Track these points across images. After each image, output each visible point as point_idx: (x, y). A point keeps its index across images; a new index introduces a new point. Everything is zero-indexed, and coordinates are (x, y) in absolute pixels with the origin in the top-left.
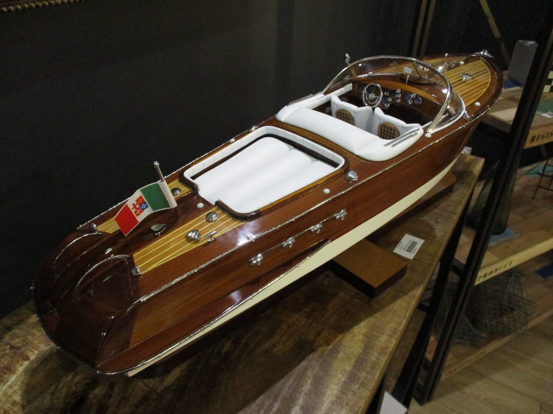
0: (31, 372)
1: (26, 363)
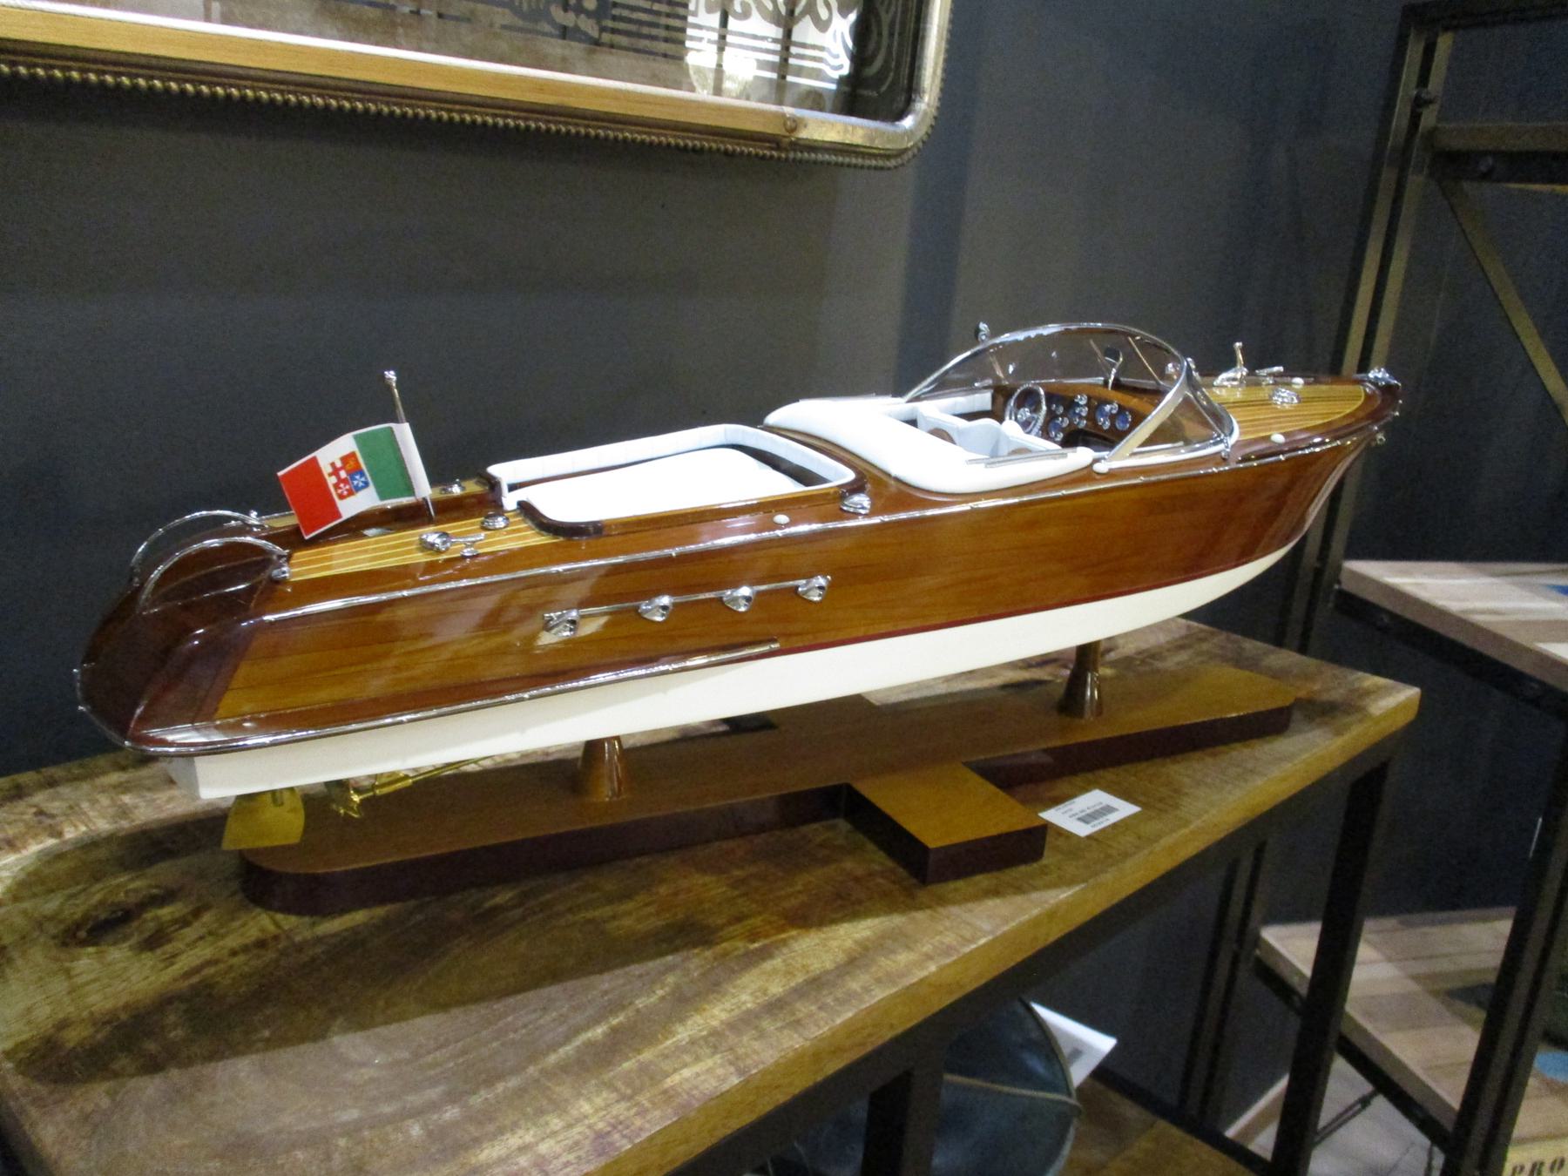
0: (56, 856)
1: (51, 842)
